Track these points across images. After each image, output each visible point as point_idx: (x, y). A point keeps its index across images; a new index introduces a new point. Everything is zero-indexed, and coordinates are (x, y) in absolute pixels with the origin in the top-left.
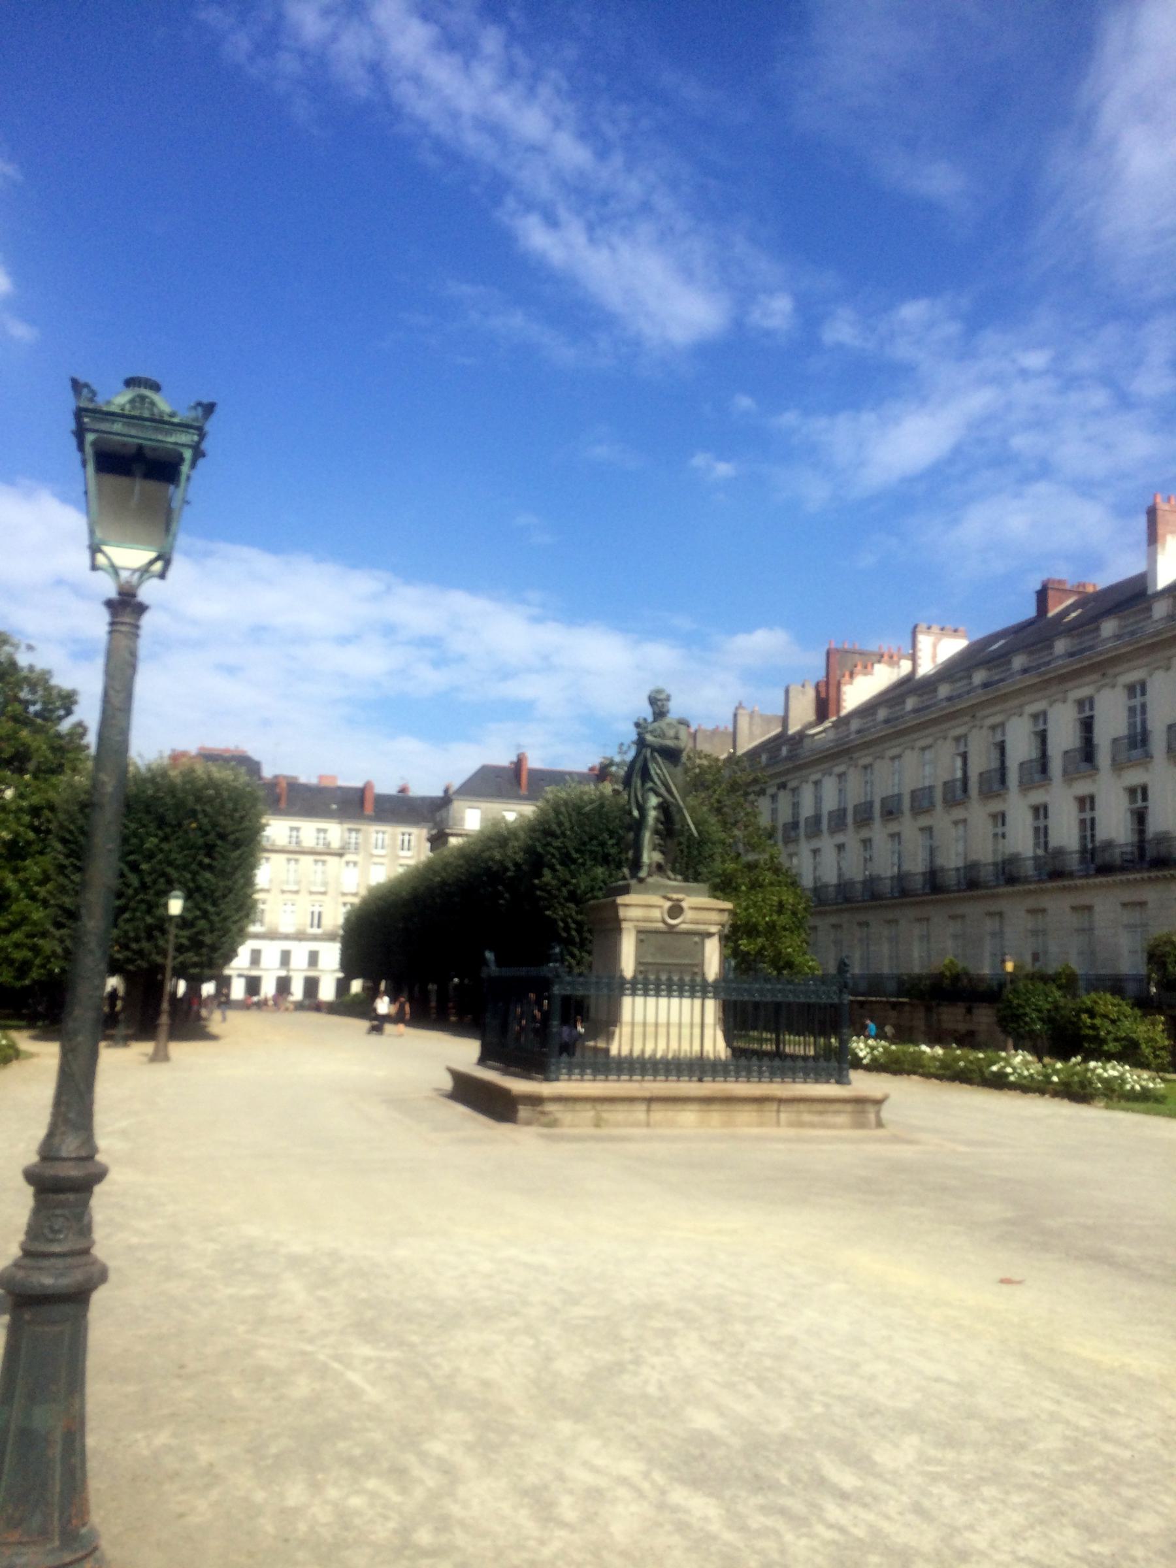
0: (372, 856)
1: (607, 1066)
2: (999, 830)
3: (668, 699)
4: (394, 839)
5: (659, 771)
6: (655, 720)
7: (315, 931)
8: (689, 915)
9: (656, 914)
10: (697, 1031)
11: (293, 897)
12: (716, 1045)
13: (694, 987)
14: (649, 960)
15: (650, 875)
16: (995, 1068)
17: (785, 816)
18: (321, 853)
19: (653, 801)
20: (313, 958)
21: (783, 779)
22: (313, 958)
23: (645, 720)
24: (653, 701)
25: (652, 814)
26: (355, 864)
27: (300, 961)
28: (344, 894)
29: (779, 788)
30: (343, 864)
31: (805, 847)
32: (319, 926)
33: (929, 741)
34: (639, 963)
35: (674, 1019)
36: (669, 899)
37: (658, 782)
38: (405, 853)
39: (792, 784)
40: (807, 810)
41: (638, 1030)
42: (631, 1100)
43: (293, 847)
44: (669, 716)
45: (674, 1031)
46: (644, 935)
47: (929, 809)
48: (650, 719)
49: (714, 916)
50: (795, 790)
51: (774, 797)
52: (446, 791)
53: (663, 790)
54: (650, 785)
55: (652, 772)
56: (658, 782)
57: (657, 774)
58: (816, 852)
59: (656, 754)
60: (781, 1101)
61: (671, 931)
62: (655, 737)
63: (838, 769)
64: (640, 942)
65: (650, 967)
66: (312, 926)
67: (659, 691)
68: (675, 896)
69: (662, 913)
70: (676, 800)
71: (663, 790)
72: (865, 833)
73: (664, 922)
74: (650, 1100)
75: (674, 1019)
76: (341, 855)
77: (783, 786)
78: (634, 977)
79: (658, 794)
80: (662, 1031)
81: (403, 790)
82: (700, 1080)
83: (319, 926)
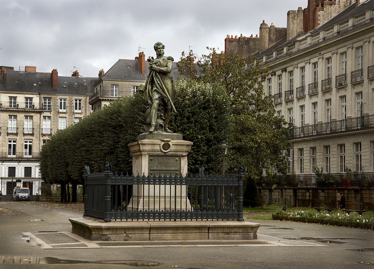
0: (59, 112)
1: (136, 215)
2: (344, 104)
3: (163, 47)
4: (71, 103)
5: (159, 82)
6: (158, 58)
7: (12, 156)
8: (172, 148)
9: (157, 148)
10: (173, 200)
11: (15, 137)
12: (185, 205)
13: (176, 180)
14: (155, 168)
15: (156, 129)
16: (43, 181)
17: (285, 87)
18: (30, 111)
19: (156, 96)
20: (28, 171)
21: (284, 66)
22: (28, 171)
23: (152, 58)
24: (156, 48)
25: (156, 102)
26: (49, 117)
27: (20, 173)
28: (44, 135)
29: (282, 72)
30: (42, 118)
31: (296, 105)
32: (14, 154)
33: (360, 44)
34: (150, 170)
35: (168, 194)
36: (163, 141)
37: (159, 87)
38: (78, 111)
39: (289, 69)
40: (297, 84)
41: (152, 199)
42: (142, 229)
43: (12, 108)
44: (164, 55)
45: (168, 200)
46: (152, 157)
47: (361, 83)
48: (155, 57)
49: (185, 148)
50: (291, 73)
51: (280, 76)
52: (101, 73)
53: (161, 91)
54: (155, 88)
55: (156, 83)
56: (159, 87)
57: (158, 83)
58: (302, 107)
59: (157, 74)
60: (209, 228)
61: (165, 155)
62: (157, 66)
63: (313, 61)
64: (150, 161)
65: (156, 172)
66: (10, 154)
67: (158, 44)
68: (165, 139)
69: (160, 147)
70: (167, 95)
71: (161, 91)
72: (327, 96)
73: (161, 151)
74: (150, 229)
75: (168, 194)
76: (40, 113)
77: (285, 70)
78: (148, 177)
79: (158, 92)
80: (162, 200)
81: (75, 74)
82: (175, 221)
83: (14, 154)
